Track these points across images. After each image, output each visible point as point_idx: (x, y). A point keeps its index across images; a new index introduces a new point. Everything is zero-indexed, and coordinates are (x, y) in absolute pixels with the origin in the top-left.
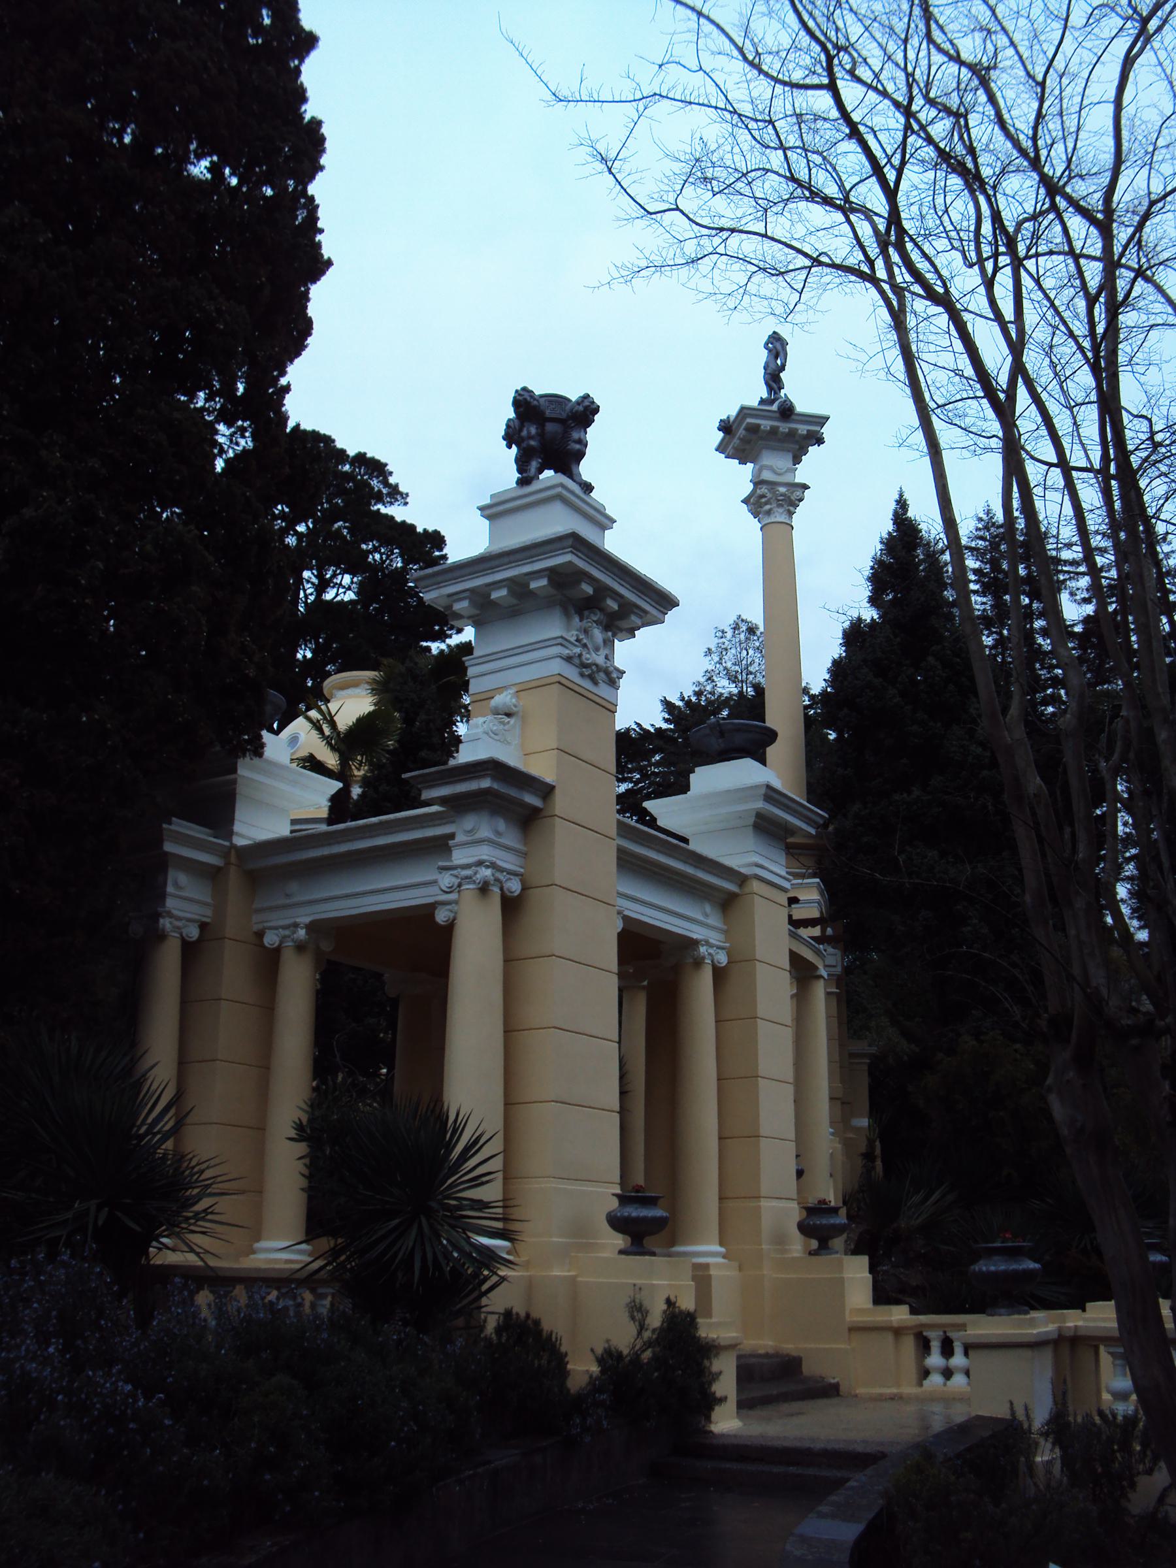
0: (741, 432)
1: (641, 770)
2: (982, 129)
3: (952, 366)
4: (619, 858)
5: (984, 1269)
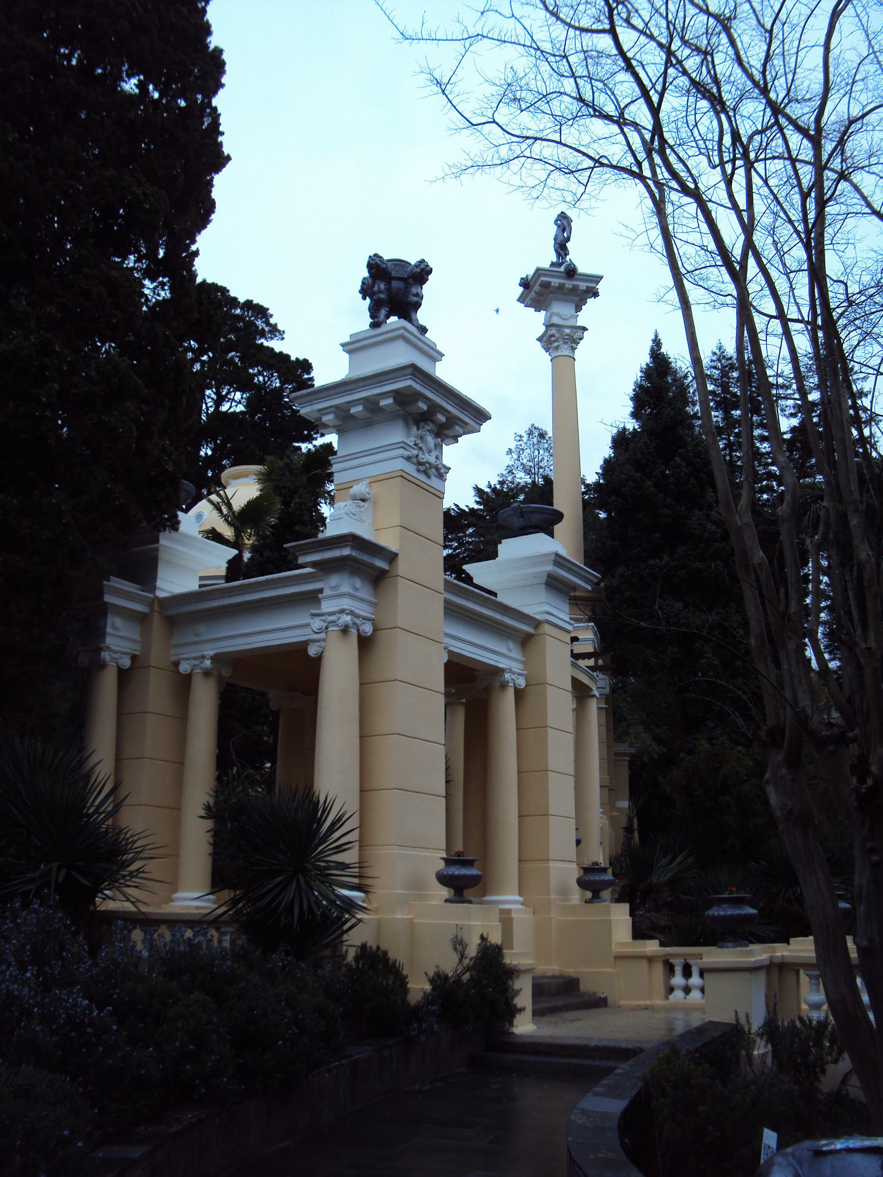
0: (537, 288)
1: (458, 540)
2: (724, 64)
3: (699, 242)
4: (445, 607)
5: (716, 913)
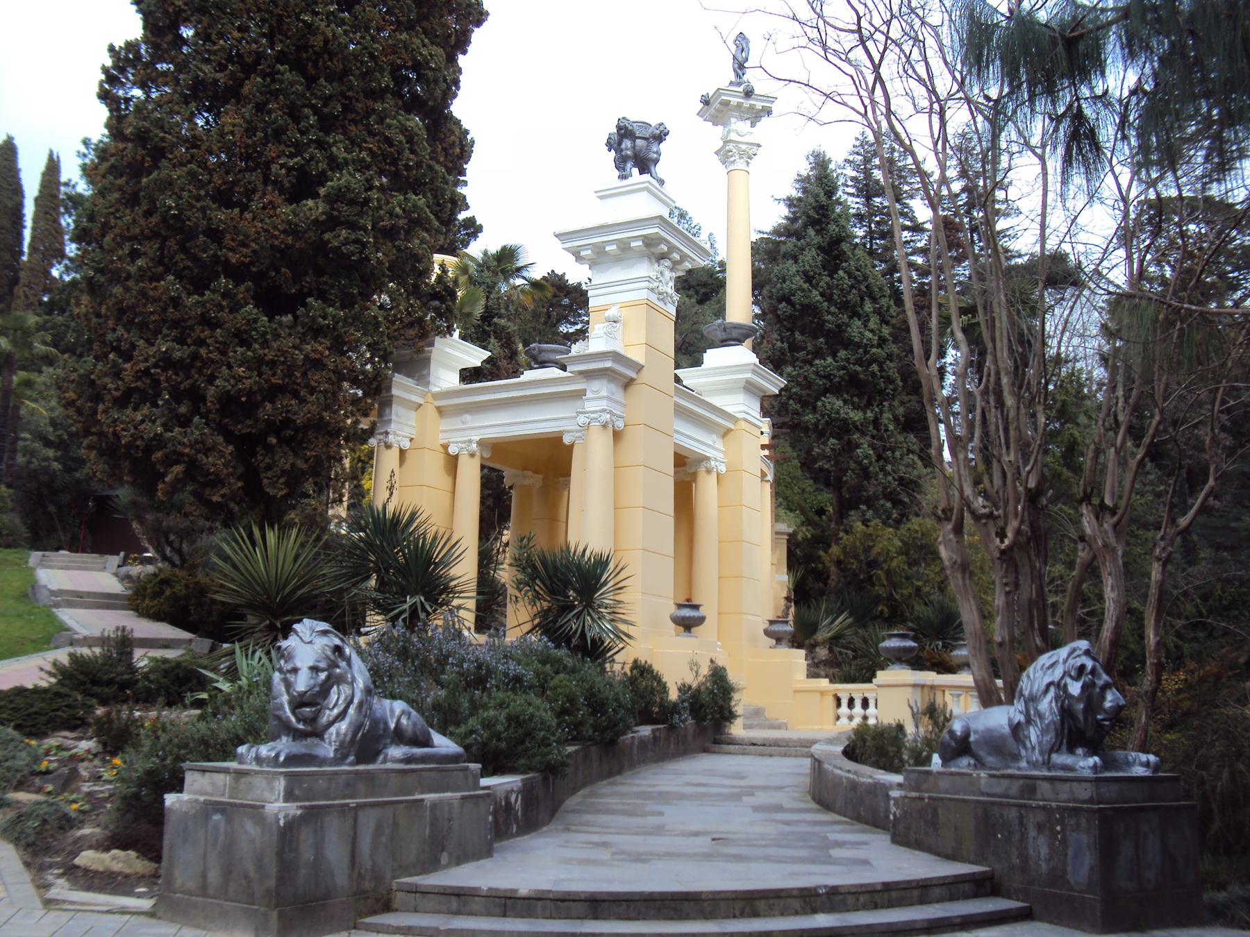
0: (716, 105)
